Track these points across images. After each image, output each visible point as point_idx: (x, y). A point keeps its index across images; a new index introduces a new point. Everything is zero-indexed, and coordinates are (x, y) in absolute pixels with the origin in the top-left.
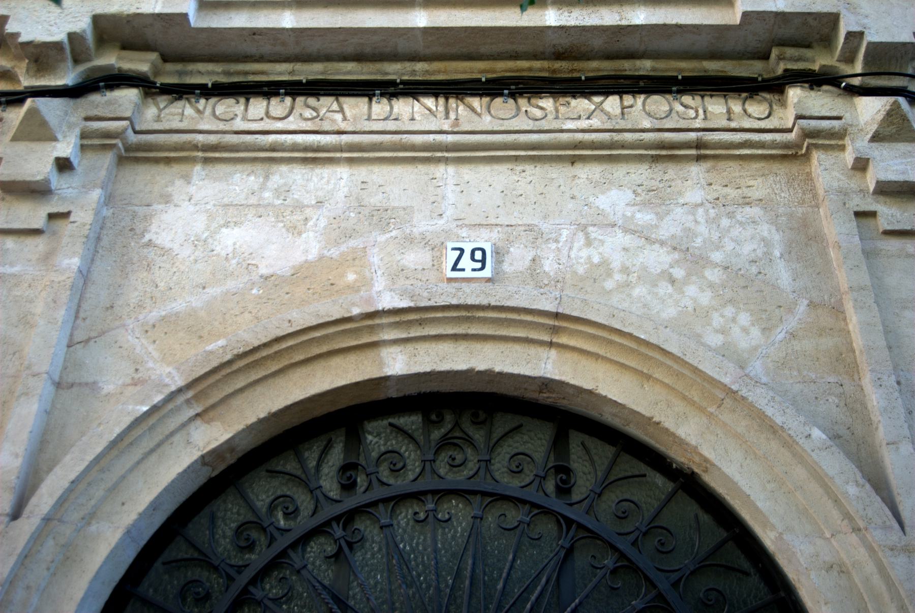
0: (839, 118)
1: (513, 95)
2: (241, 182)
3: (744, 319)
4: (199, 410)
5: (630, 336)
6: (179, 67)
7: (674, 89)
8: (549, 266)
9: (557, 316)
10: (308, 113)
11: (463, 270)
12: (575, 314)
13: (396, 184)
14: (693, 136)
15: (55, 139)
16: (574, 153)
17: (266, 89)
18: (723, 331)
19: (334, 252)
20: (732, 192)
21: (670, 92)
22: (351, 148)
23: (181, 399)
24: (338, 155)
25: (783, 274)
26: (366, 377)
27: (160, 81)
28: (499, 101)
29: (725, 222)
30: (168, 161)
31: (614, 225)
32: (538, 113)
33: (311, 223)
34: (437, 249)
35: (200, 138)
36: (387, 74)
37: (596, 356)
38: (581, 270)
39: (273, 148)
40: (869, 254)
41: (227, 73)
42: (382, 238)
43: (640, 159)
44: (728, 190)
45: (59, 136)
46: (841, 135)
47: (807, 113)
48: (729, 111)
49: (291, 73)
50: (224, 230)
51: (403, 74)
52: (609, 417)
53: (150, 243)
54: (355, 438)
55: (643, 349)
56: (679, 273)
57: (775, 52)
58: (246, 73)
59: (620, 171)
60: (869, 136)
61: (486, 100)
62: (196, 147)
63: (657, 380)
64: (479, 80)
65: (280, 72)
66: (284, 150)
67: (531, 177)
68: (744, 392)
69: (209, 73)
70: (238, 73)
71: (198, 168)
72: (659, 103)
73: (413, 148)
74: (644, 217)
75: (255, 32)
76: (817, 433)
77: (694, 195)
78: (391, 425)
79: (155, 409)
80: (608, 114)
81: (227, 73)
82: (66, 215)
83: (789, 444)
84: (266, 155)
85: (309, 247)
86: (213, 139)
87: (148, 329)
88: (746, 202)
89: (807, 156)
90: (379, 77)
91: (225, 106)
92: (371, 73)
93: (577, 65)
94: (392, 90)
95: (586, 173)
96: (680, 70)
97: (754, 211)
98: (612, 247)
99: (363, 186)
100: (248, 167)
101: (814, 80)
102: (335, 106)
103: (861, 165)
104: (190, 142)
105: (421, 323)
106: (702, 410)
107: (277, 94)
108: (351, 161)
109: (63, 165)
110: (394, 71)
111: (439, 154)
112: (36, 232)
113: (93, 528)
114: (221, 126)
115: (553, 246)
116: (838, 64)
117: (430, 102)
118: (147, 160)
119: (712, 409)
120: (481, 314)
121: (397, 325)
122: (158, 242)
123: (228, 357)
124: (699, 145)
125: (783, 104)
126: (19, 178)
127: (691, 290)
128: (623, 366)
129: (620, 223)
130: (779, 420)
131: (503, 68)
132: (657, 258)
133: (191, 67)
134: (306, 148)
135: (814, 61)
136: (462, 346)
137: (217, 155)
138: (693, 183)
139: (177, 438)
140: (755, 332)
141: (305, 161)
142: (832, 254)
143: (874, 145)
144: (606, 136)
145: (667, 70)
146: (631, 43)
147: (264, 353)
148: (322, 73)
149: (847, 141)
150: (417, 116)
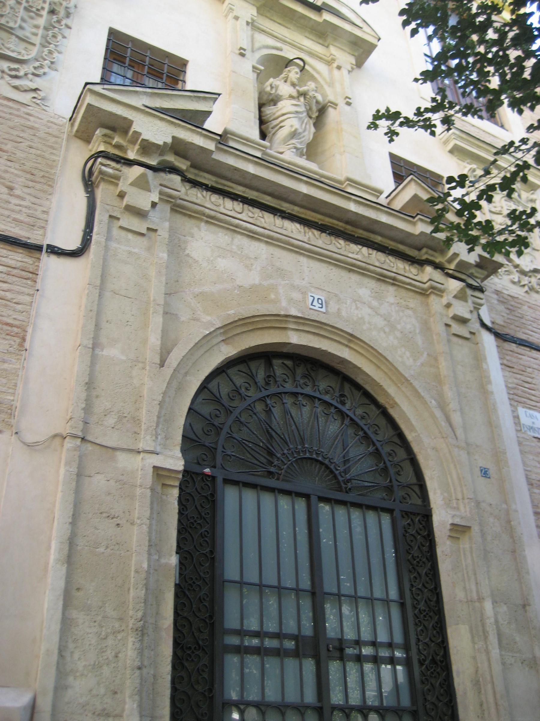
0: (442, 284)
1: (329, 234)
2: (222, 238)
3: (408, 354)
4: (224, 338)
5: (376, 350)
6: (196, 171)
7: (387, 252)
8: (344, 313)
9: (352, 335)
10: (250, 214)
11: (315, 306)
12: (358, 336)
13: (286, 260)
14: (393, 275)
15: (150, 191)
16: (352, 268)
17: (232, 196)
18: (401, 357)
19: (265, 283)
20: (404, 303)
21: (385, 252)
22: (269, 237)
23: (219, 332)
24: (262, 238)
25: (419, 340)
26: (284, 342)
27: (189, 176)
28: (324, 234)
29: (401, 314)
30: (190, 216)
31: (365, 303)
32: (339, 246)
33: (254, 267)
34: (304, 293)
35: (207, 211)
36: (282, 207)
37: (362, 355)
38: (355, 319)
39: (237, 226)
40: (449, 341)
41: (216, 182)
42: (283, 283)
43: (373, 278)
44: (402, 301)
45: (152, 191)
46: (442, 291)
47: (433, 279)
48: (405, 268)
49: (244, 192)
50: (219, 259)
51: (288, 209)
52: (360, 380)
53: (188, 255)
54: (269, 365)
55: (379, 357)
56: (387, 330)
57: (425, 250)
58: (225, 185)
59: (366, 280)
60: (453, 295)
61: (319, 232)
62: (204, 214)
63: (382, 370)
64: (317, 223)
65: (239, 190)
66: (241, 229)
67: (336, 273)
68: (412, 381)
69: (209, 179)
70: (222, 184)
71: (203, 224)
72: (381, 256)
73: (292, 245)
74: (375, 303)
75: (236, 169)
76: (433, 402)
77: (391, 299)
78: (283, 363)
79: (210, 333)
80: (363, 255)
81: (216, 182)
82: (156, 231)
83: (425, 403)
84: (234, 229)
85: (253, 278)
86: (212, 213)
87: (196, 296)
88: (407, 308)
89: (428, 296)
90: (278, 207)
91: (215, 198)
92: (275, 204)
93: (354, 229)
94: (283, 215)
95: (355, 278)
96: (390, 245)
97: (410, 312)
98: (365, 311)
99: (272, 256)
100: (225, 231)
101: (437, 266)
102: (261, 215)
103: (448, 306)
104: (202, 211)
105: (304, 324)
106: (396, 384)
107: (237, 200)
108: (267, 242)
109: (154, 205)
110: (286, 207)
111: (302, 252)
112: (142, 235)
113: (188, 378)
114: (215, 208)
115: (345, 306)
116: (445, 262)
117: (298, 226)
118: (181, 213)
119: (399, 385)
120: (325, 327)
121: (296, 323)
122: (192, 256)
123: (236, 319)
124: (394, 279)
125: (423, 271)
126: (137, 206)
127: (391, 338)
128: (371, 361)
129: (367, 303)
130: (422, 394)
131: (328, 221)
132: (380, 322)
133: (202, 173)
134: (250, 231)
135: (436, 258)
136: (316, 338)
137: (212, 221)
138: (390, 293)
139: (215, 348)
140: (411, 360)
141: (248, 236)
142: (435, 337)
143: (454, 299)
144: (363, 265)
145: (384, 243)
146: (377, 228)
147: (249, 321)
148: (256, 197)
149: (444, 294)
150: (294, 231)
